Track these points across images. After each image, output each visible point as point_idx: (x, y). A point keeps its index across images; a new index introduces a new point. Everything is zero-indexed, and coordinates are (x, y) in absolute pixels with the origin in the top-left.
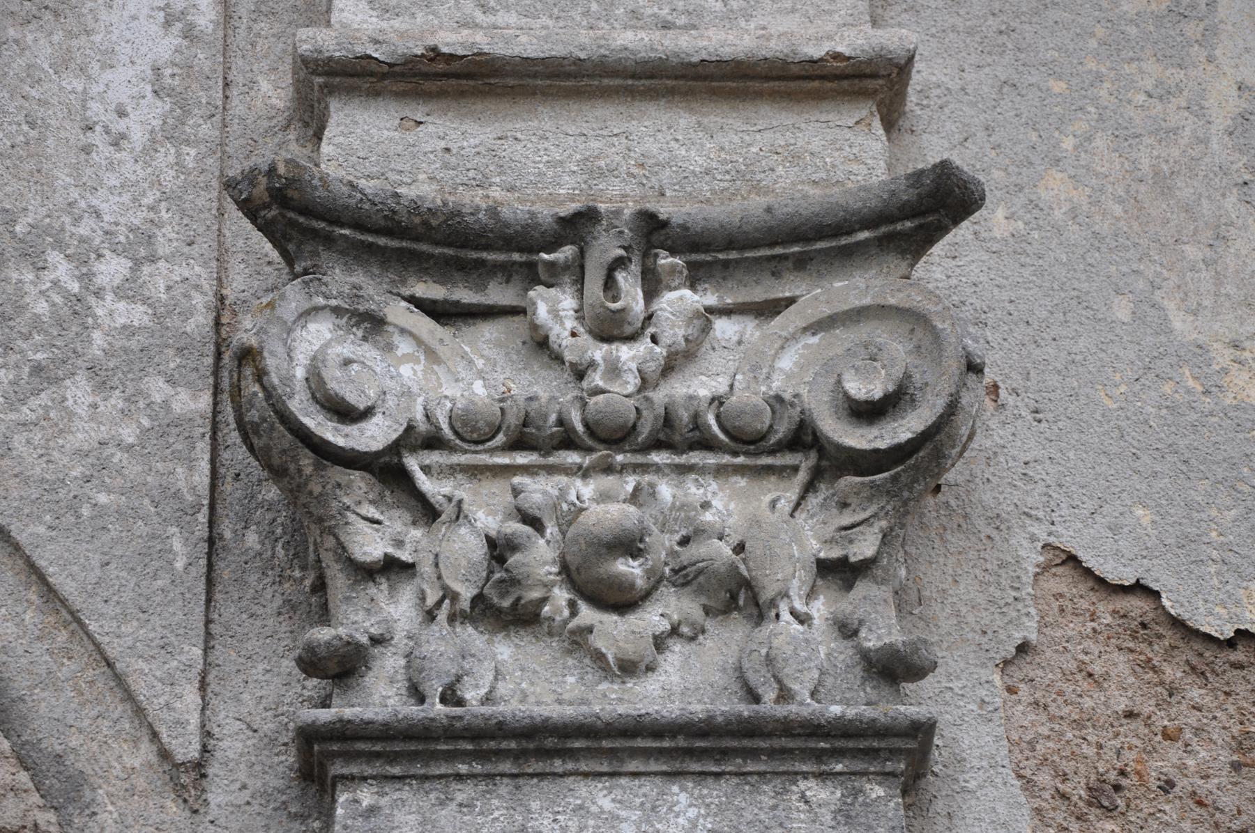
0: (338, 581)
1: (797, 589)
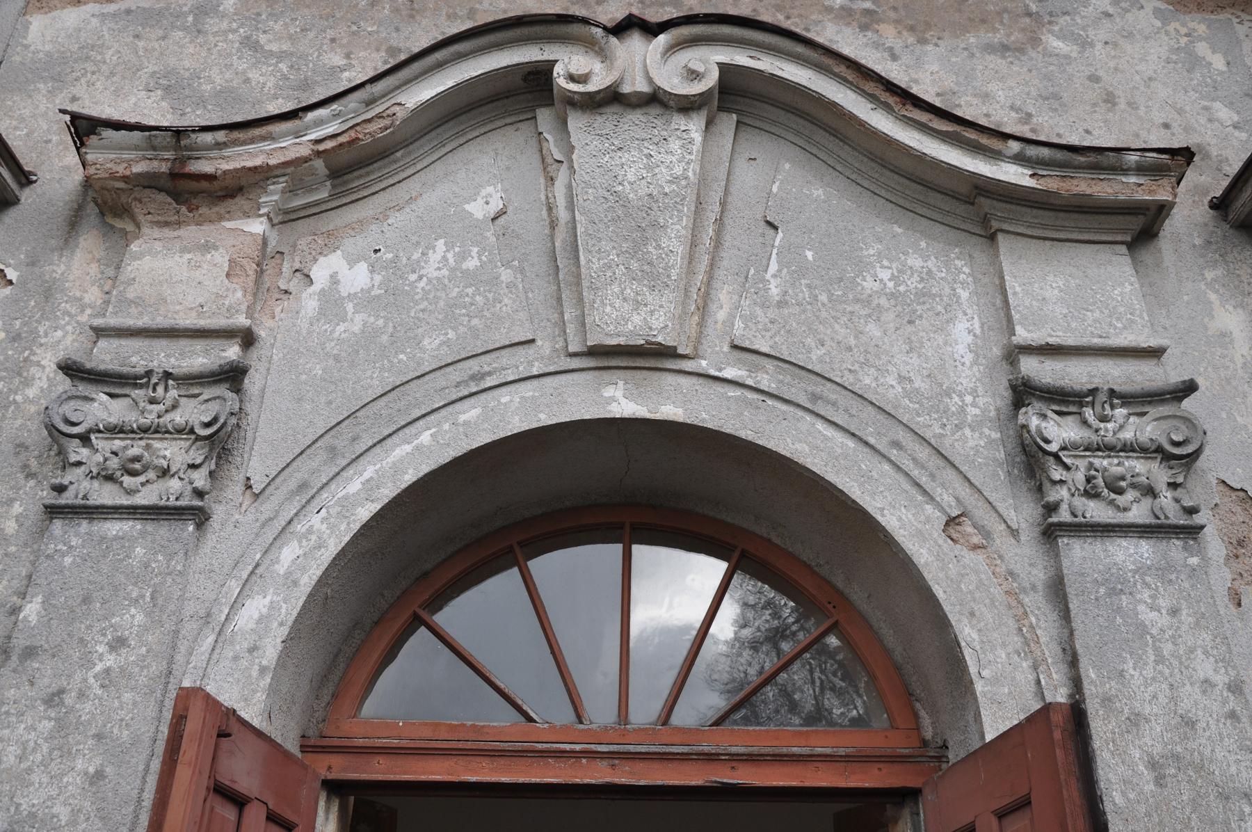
0: (1047, 485)
1: (1164, 489)
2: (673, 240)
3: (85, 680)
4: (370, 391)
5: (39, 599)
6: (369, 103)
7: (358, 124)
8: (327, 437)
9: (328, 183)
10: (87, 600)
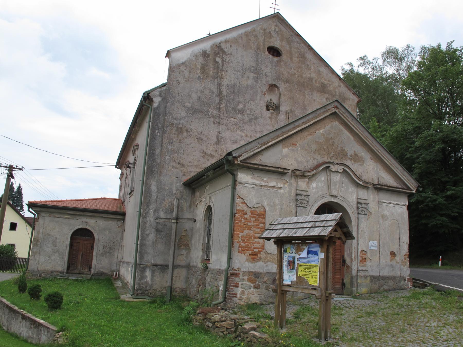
2: (337, 186)
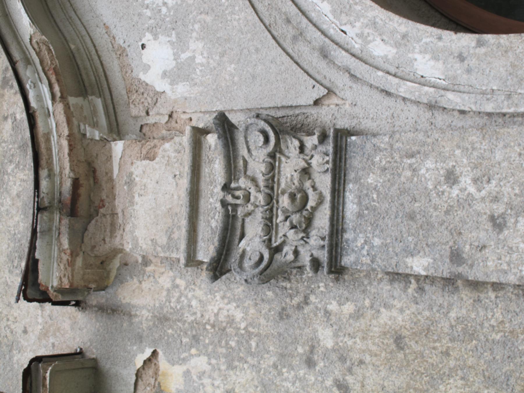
3: (483, 199)
4: (249, 18)
5: (409, 261)
6: (28, 61)
7: (43, 70)
8: (285, 45)
9: (90, 98)
10: (411, 217)
